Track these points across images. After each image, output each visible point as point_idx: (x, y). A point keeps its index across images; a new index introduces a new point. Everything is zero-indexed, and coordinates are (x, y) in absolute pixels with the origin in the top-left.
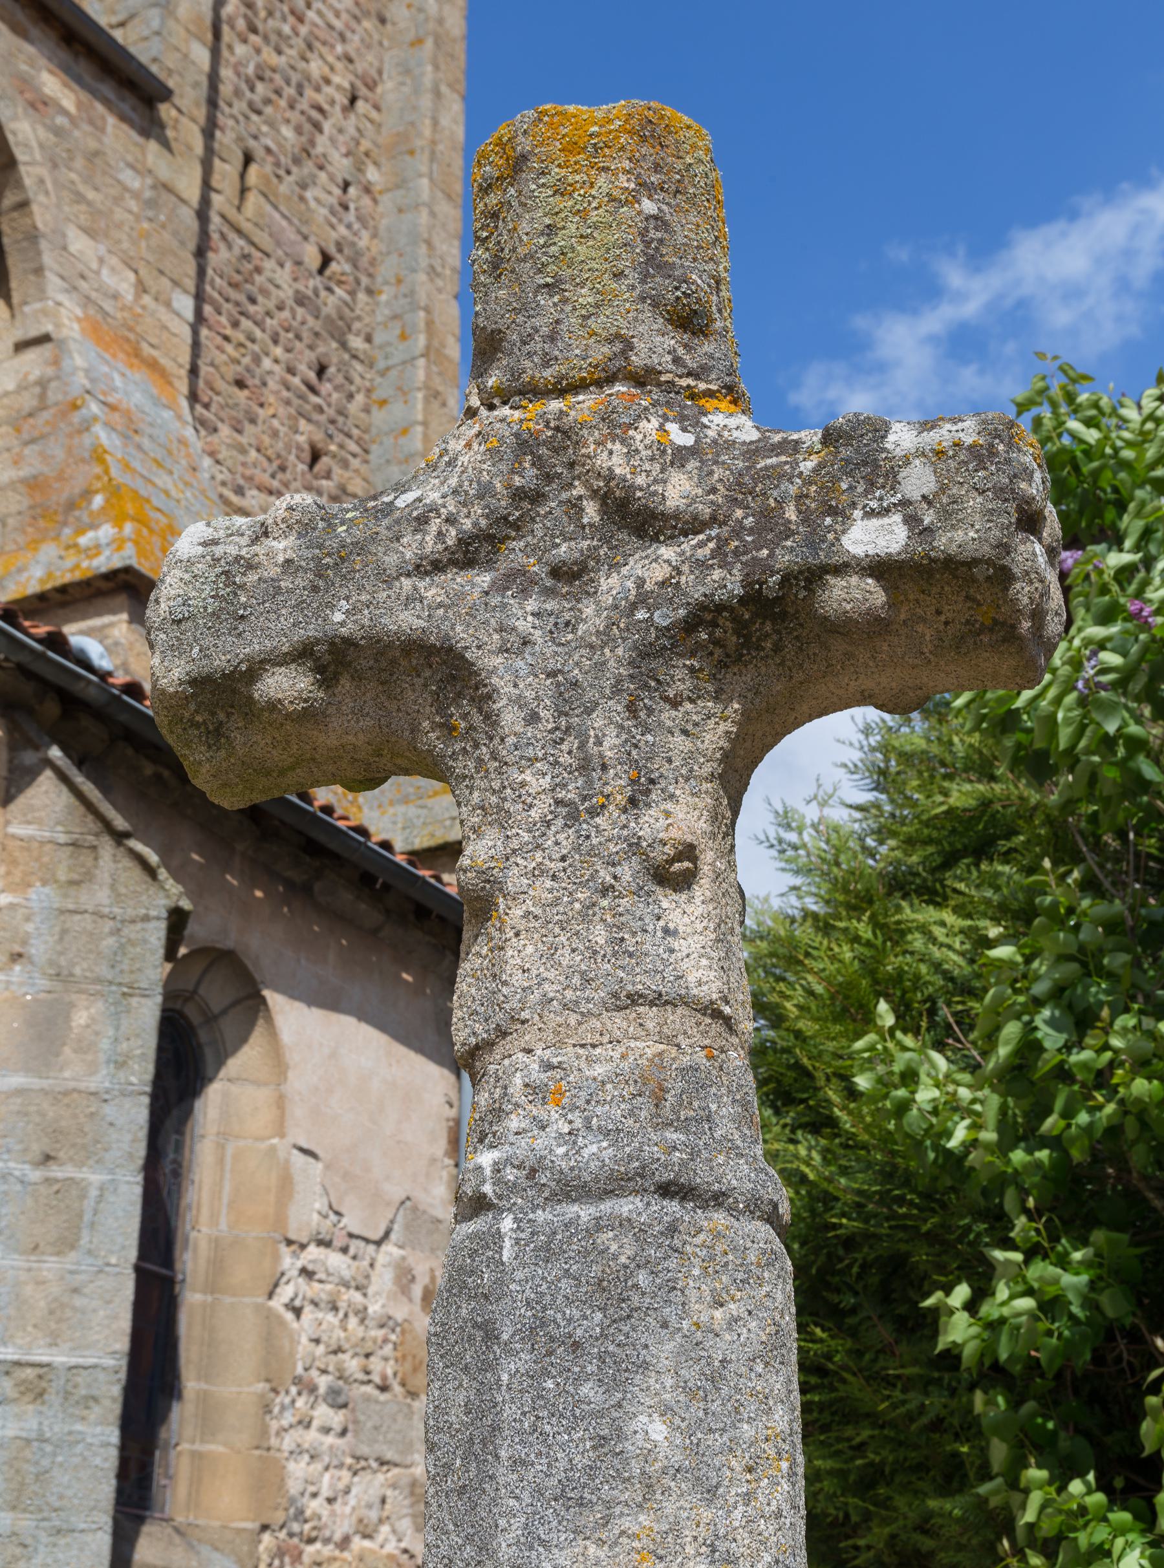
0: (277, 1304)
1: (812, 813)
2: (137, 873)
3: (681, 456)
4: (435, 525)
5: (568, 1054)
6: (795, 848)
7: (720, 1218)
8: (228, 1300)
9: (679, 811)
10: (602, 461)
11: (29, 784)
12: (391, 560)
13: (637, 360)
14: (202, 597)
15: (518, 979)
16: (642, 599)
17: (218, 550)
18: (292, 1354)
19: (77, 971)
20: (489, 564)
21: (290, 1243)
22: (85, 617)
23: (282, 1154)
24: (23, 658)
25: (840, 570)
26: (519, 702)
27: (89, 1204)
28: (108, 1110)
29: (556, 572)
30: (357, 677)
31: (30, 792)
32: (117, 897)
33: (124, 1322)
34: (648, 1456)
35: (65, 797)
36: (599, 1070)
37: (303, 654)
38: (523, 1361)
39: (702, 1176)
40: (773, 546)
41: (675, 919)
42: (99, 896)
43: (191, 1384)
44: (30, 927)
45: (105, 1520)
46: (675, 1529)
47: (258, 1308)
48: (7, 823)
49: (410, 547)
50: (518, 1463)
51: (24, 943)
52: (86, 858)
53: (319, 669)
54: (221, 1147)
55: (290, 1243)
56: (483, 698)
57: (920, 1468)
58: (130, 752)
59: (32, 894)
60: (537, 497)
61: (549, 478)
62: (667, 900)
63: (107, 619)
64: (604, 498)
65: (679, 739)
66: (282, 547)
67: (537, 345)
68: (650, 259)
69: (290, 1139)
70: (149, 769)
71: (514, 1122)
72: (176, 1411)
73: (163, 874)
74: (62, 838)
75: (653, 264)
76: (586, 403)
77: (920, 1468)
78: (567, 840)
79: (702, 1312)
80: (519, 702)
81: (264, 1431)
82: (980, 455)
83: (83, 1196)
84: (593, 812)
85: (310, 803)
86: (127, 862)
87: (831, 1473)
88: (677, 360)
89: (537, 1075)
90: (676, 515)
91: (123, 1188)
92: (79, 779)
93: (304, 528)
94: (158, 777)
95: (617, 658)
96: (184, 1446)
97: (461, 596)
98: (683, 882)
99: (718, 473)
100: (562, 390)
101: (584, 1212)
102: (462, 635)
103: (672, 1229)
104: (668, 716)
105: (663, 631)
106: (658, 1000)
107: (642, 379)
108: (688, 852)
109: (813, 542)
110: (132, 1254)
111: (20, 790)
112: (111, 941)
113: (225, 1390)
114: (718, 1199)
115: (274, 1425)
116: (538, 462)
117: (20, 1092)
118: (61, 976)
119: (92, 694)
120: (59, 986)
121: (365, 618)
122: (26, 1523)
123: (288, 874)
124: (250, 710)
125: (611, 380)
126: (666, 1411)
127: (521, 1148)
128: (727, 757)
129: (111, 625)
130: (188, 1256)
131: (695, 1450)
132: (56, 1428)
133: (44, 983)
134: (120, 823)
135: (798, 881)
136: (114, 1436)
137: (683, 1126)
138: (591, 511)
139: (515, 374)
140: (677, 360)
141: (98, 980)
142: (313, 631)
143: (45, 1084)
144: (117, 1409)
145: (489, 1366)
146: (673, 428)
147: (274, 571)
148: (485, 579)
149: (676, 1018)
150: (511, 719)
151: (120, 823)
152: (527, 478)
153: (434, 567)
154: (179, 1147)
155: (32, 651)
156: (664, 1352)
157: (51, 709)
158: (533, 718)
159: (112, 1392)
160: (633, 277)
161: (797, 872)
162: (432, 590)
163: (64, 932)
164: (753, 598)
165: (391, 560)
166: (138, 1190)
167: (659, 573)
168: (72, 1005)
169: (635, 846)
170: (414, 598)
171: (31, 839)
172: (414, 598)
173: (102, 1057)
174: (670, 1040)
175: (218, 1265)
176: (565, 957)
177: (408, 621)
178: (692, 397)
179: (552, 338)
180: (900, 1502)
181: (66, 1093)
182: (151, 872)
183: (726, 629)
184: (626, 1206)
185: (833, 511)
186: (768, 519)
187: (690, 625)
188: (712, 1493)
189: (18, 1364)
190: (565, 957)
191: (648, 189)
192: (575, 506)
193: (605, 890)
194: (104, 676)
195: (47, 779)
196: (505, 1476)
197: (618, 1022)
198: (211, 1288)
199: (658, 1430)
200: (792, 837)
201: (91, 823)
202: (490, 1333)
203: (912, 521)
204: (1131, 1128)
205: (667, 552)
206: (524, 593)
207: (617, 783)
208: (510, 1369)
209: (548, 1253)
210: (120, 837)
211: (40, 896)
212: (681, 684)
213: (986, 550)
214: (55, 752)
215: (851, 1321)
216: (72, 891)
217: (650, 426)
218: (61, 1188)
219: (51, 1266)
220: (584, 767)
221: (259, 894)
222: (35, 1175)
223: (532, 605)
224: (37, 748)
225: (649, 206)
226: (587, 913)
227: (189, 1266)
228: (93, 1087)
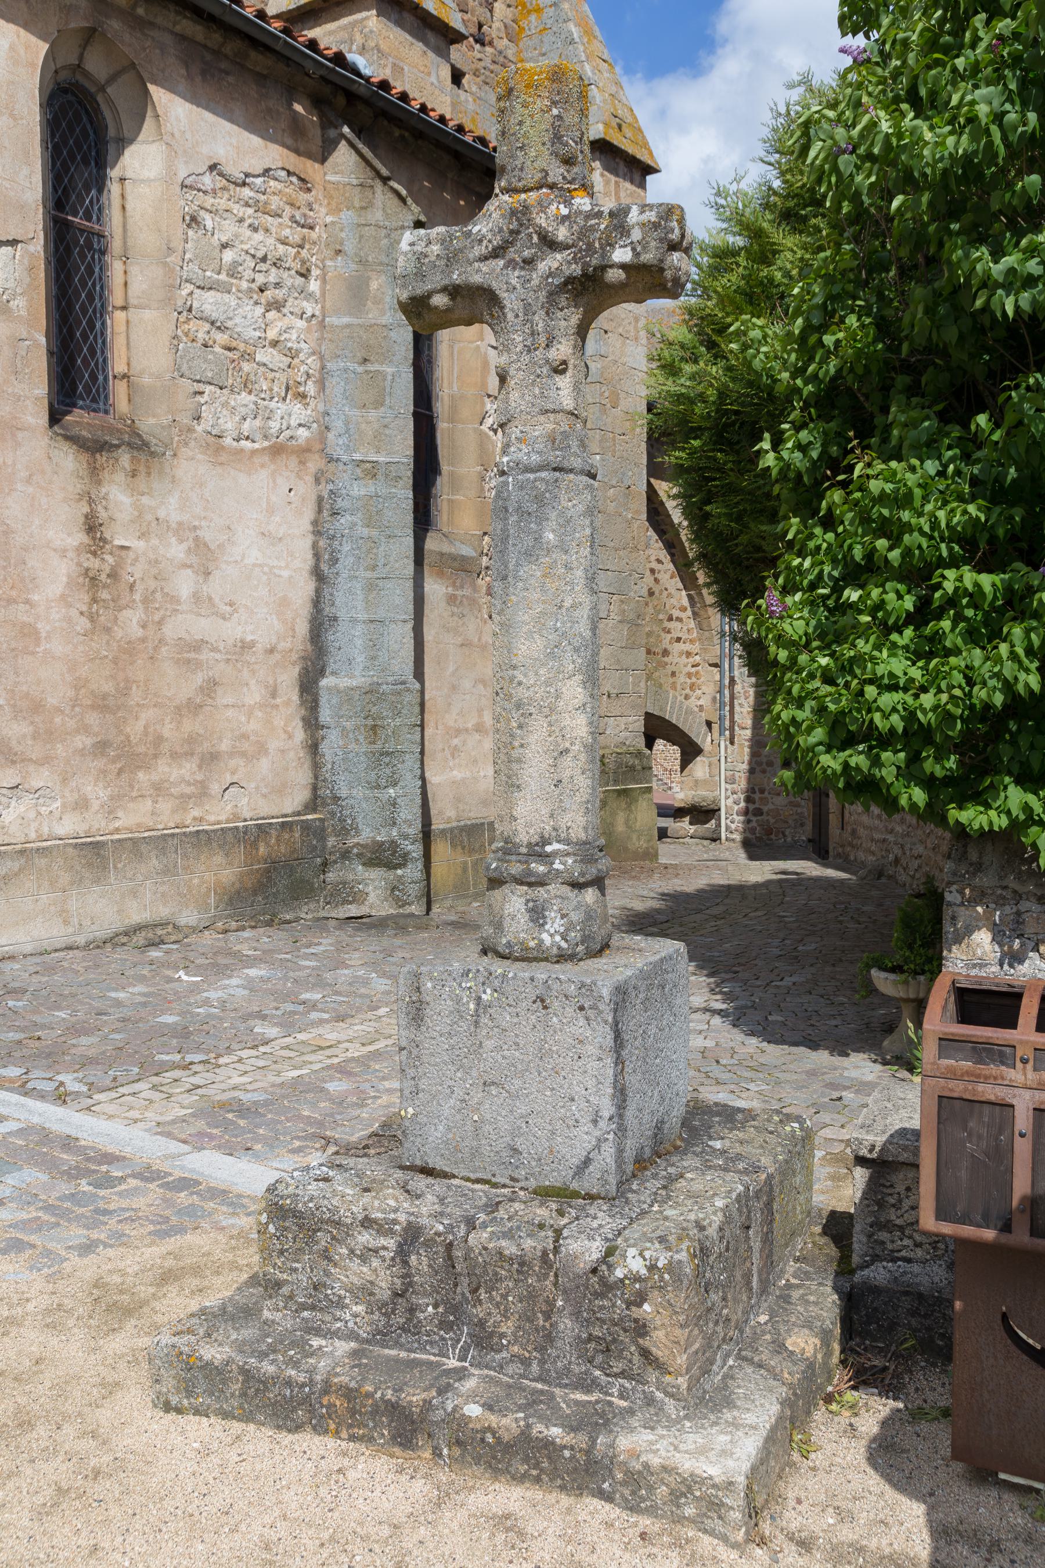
0: (485, 427)
1: (734, 187)
2: (396, 201)
3: (564, 219)
4: (485, 242)
5: (527, 428)
6: (723, 207)
7: (572, 476)
8: (460, 426)
9: (562, 348)
10: (538, 221)
11: (334, 150)
12: (471, 256)
13: (550, 180)
14: (411, 268)
15: (513, 404)
16: (550, 274)
17: (415, 248)
18: (494, 452)
19: (370, 259)
20: (503, 257)
21: (489, 396)
22: (351, 14)
23: (483, 350)
24: (323, 72)
25: (611, 266)
26: (512, 310)
27: (388, 383)
28: (392, 334)
29: (524, 261)
30: (463, 297)
31: (335, 154)
32: (387, 216)
33: (410, 441)
34: (548, 543)
35: (354, 157)
36: (537, 433)
37: (444, 289)
38: (514, 518)
39: (566, 464)
40: (591, 256)
41: (560, 384)
42: (377, 215)
43: (445, 467)
44: (343, 235)
45: (410, 532)
46: (555, 562)
47: (475, 430)
48: (325, 174)
49: (479, 250)
50: (514, 545)
51: (342, 244)
52: (368, 193)
53: (450, 294)
54: (451, 347)
55: (489, 396)
56: (502, 308)
57: (762, 511)
58: (386, 123)
59: (342, 215)
60: (518, 232)
61: (521, 225)
62: (558, 378)
63: (364, 14)
64: (539, 234)
65: (563, 322)
66: (436, 248)
67: (516, 173)
68: (555, 135)
69: (486, 342)
70: (397, 133)
71: (512, 449)
72: (439, 479)
73: (409, 201)
74: (355, 182)
75: (557, 138)
76: (533, 195)
77: (762, 511)
78: (527, 358)
79: (564, 503)
80: (512, 310)
81: (482, 489)
82: (656, 226)
83: (385, 380)
84: (536, 349)
85: (487, 146)
86: (390, 195)
87: (725, 514)
88: (564, 178)
89: (519, 435)
90: (561, 243)
91: (404, 375)
92: (360, 146)
93: (443, 242)
94: (402, 137)
95: (542, 295)
96: (444, 497)
97: (494, 270)
98: (563, 372)
99: (575, 227)
100: (526, 190)
101: (532, 476)
102: (495, 285)
103: (556, 481)
104: (559, 314)
105: (557, 286)
106: (554, 411)
107: (552, 187)
108: (564, 362)
109: (603, 256)
110: (411, 408)
111: (330, 154)
112: (385, 241)
113: (462, 470)
114: (571, 471)
115: (487, 486)
116: (518, 219)
117: (348, 326)
118: (362, 262)
119: (362, 91)
120: (361, 268)
121: (463, 277)
122: (374, 533)
123: (477, 189)
124: (429, 308)
125: (541, 187)
126: (553, 531)
127: (515, 457)
128: (579, 326)
129: (367, 18)
130: (439, 404)
131: (562, 541)
132: (383, 491)
133: (354, 266)
134: (385, 172)
135: (725, 225)
136: (410, 494)
137: (561, 449)
138: (535, 239)
139: (510, 184)
140: (564, 178)
141: (381, 264)
142: (446, 282)
143: (360, 321)
144: (411, 482)
145: (506, 519)
146: (562, 206)
147: (433, 258)
148: (501, 263)
149: (559, 416)
150: (510, 316)
151: (385, 172)
152: (514, 225)
153: (484, 258)
154: (430, 347)
155: (327, 67)
156: (553, 515)
157: (341, 101)
158: (517, 316)
159: (407, 474)
160: (549, 144)
161: (723, 221)
162: (484, 267)
163: (361, 237)
164: (585, 275)
165: (471, 256)
166: (411, 376)
167: (556, 265)
168: (369, 278)
169: (547, 361)
170: (478, 271)
171: (339, 182)
172: (478, 271)
173: (387, 307)
174: (558, 424)
175: (454, 409)
176: (527, 398)
177: (477, 279)
178: (570, 191)
179: (522, 169)
180: (752, 525)
181: (371, 326)
182: (403, 200)
183: (577, 285)
184: (544, 474)
185: (610, 245)
186: (590, 246)
187: (565, 283)
188: (566, 552)
189: (362, 461)
190: (527, 398)
191: (554, 103)
192: (530, 236)
193: (538, 376)
194: (367, 79)
195: (343, 146)
196: (511, 548)
197: (542, 418)
198: (451, 420)
199: (551, 536)
200: (722, 202)
201: (370, 173)
202: (507, 511)
203: (634, 249)
204: (677, 456)
205: (558, 256)
206: (514, 269)
207: (542, 340)
208: (513, 519)
209: (521, 488)
210: (385, 180)
211: (347, 216)
212: (563, 303)
213: (655, 262)
214: (346, 130)
215: (737, 447)
216: (363, 213)
217: (553, 207)
218: (374, 375)
219: (373, 414)
220: (532, 334)
221: (462, 203)
222: (360, 369)
223: (516, 273)
224: (336, 127)
225: (555, 111)
226: (533, 384)
227: (440, 410)
228: (384, 322)
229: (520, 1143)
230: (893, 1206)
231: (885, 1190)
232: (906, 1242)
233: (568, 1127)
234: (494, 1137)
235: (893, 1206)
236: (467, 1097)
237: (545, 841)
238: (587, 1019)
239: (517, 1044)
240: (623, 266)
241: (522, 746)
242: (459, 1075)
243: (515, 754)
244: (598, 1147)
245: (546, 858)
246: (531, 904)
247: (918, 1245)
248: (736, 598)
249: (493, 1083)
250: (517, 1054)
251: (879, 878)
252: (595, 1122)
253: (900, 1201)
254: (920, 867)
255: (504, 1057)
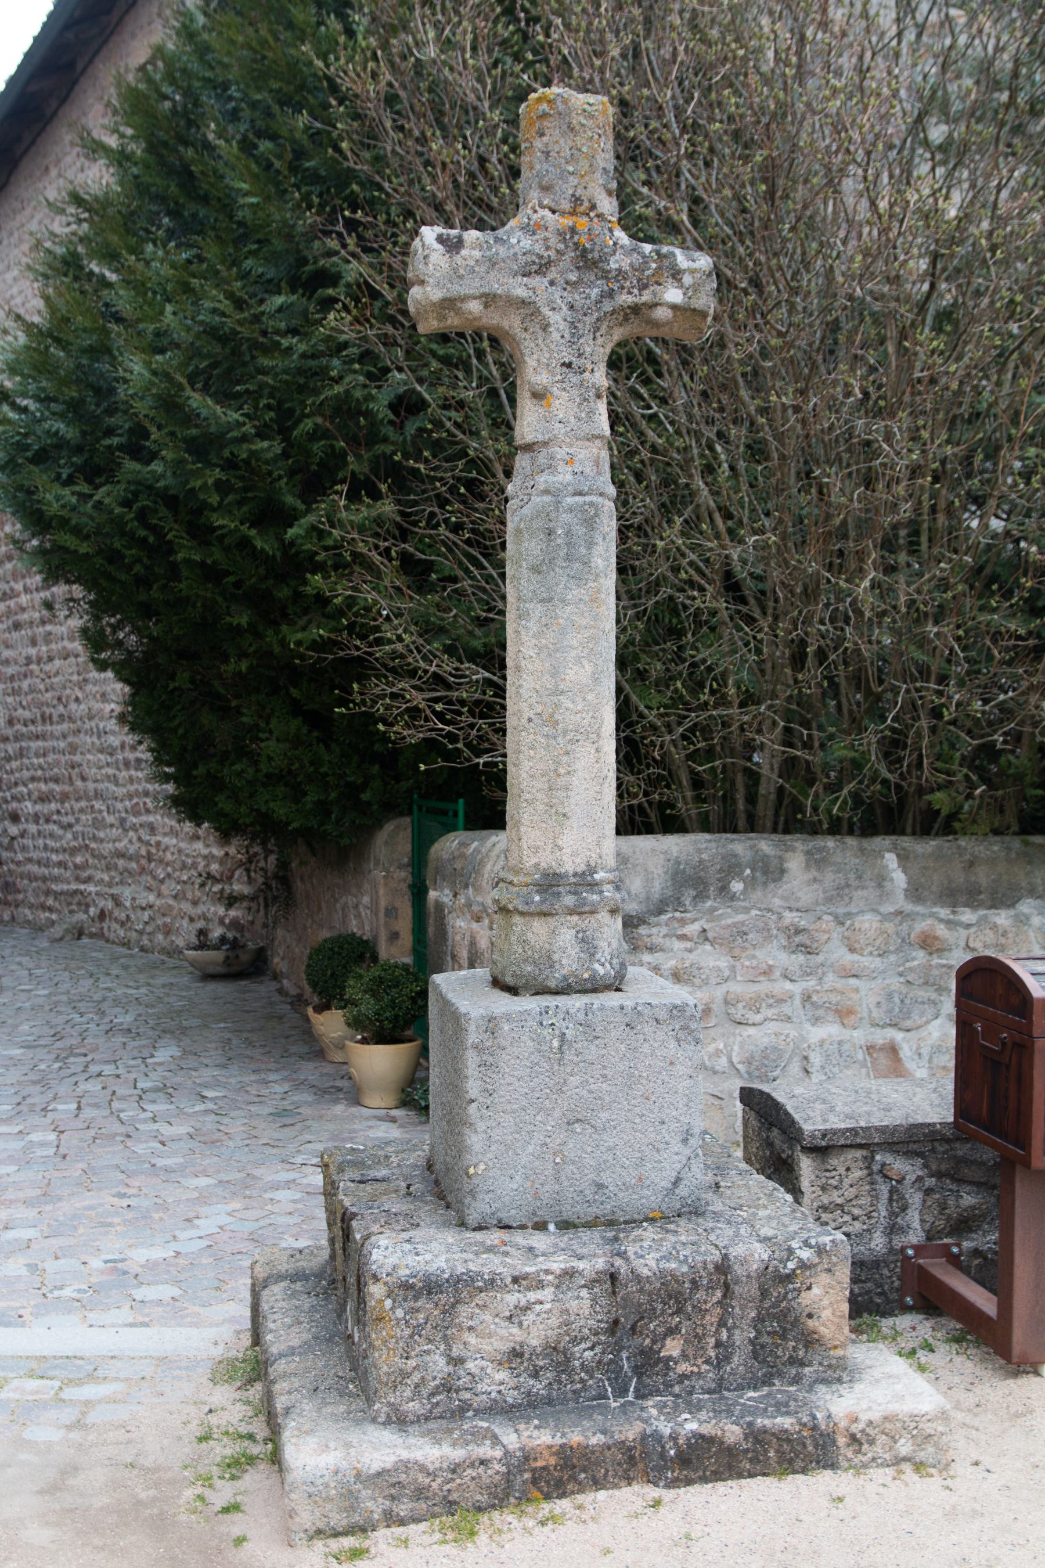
229: (606, 1178)
230: (835, 1187)
231: (828, 1174)
232: (847, 1218)
233: (658, 1151)
234: (578, 1176)
235: (835, 1187)
236: (548, 1140)
237: (592, 870)
238: (678, 1040)
239: (604, 1076)
240: (674, 307)
241: (569, 773)
242: (539, 1118)
243: (562, 781)
244: (687, 1166)
245: (593, 886)
246: (580, 935)
247: (855, 1219)
248: (105, 612)
249: (578, 1121)
250: (604, 1086)
251: (79, 938)
252: (685, 1141)
253: (841, 1181)
254: (151, 918)
255: (590, 1092)
